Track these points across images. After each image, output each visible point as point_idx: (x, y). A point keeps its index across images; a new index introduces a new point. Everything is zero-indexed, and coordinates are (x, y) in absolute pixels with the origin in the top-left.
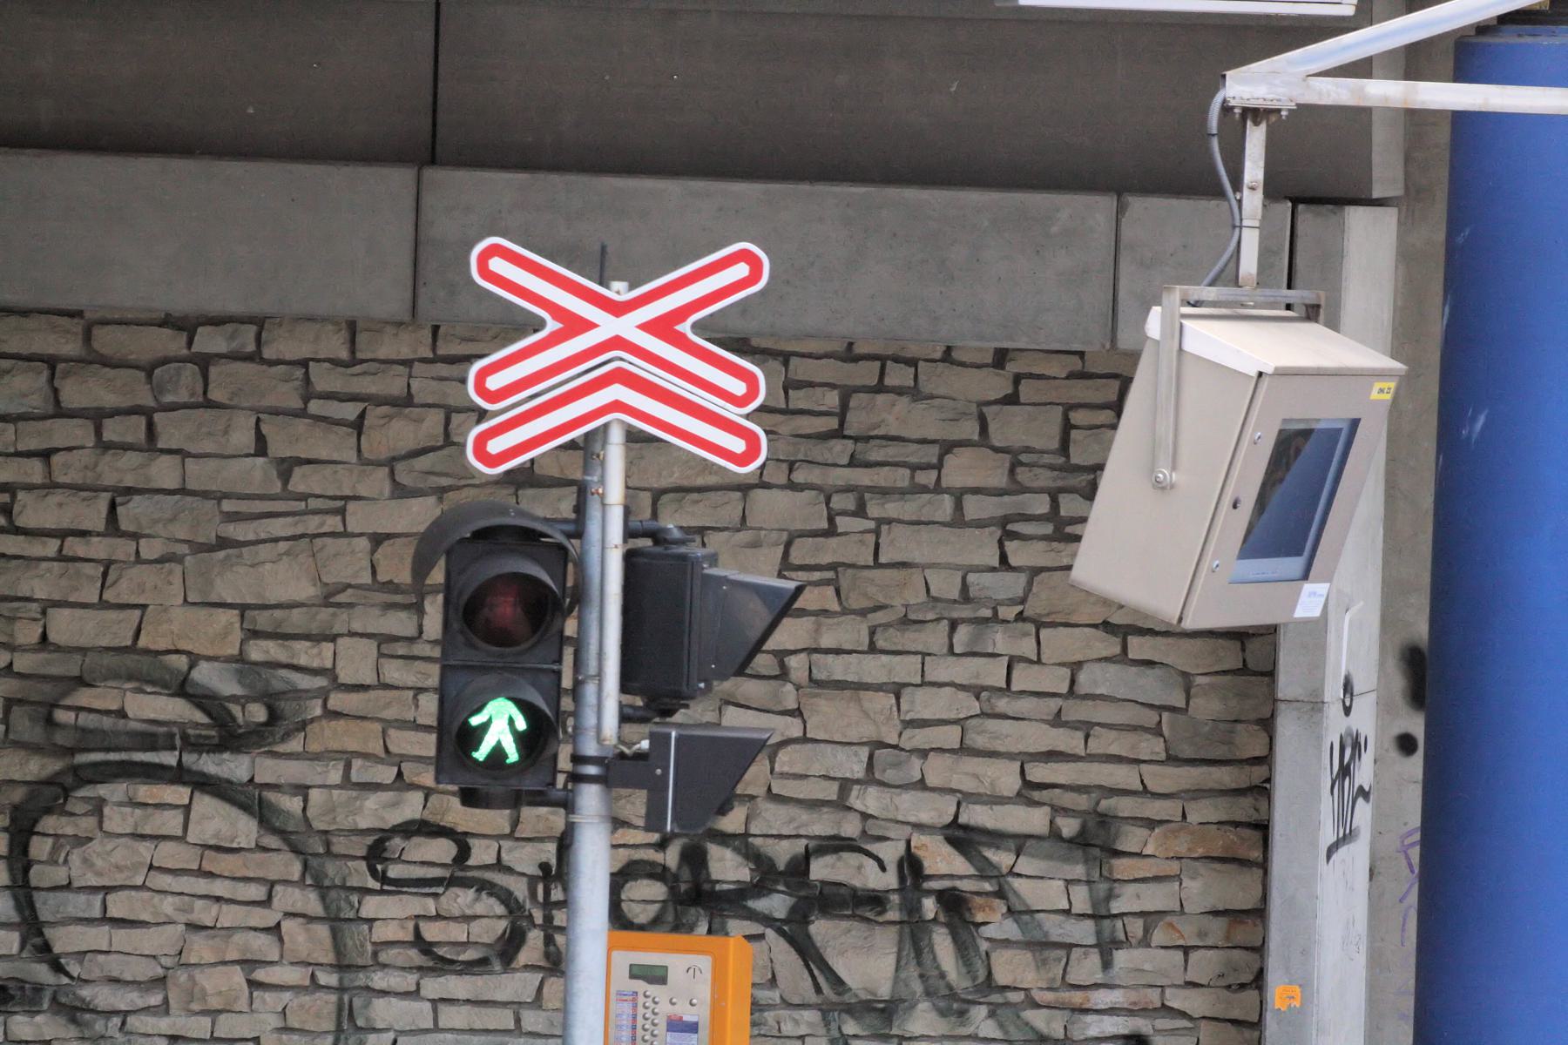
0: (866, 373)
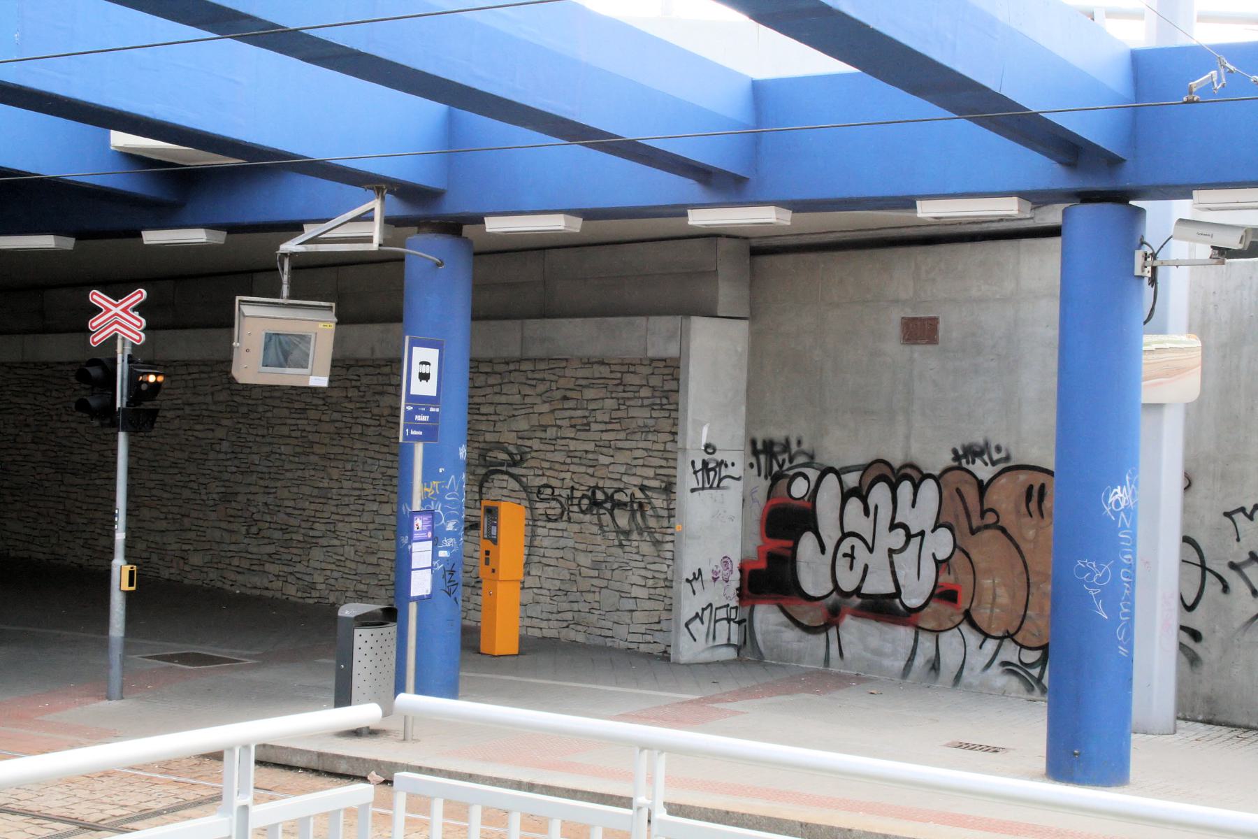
0: (625, 368)
